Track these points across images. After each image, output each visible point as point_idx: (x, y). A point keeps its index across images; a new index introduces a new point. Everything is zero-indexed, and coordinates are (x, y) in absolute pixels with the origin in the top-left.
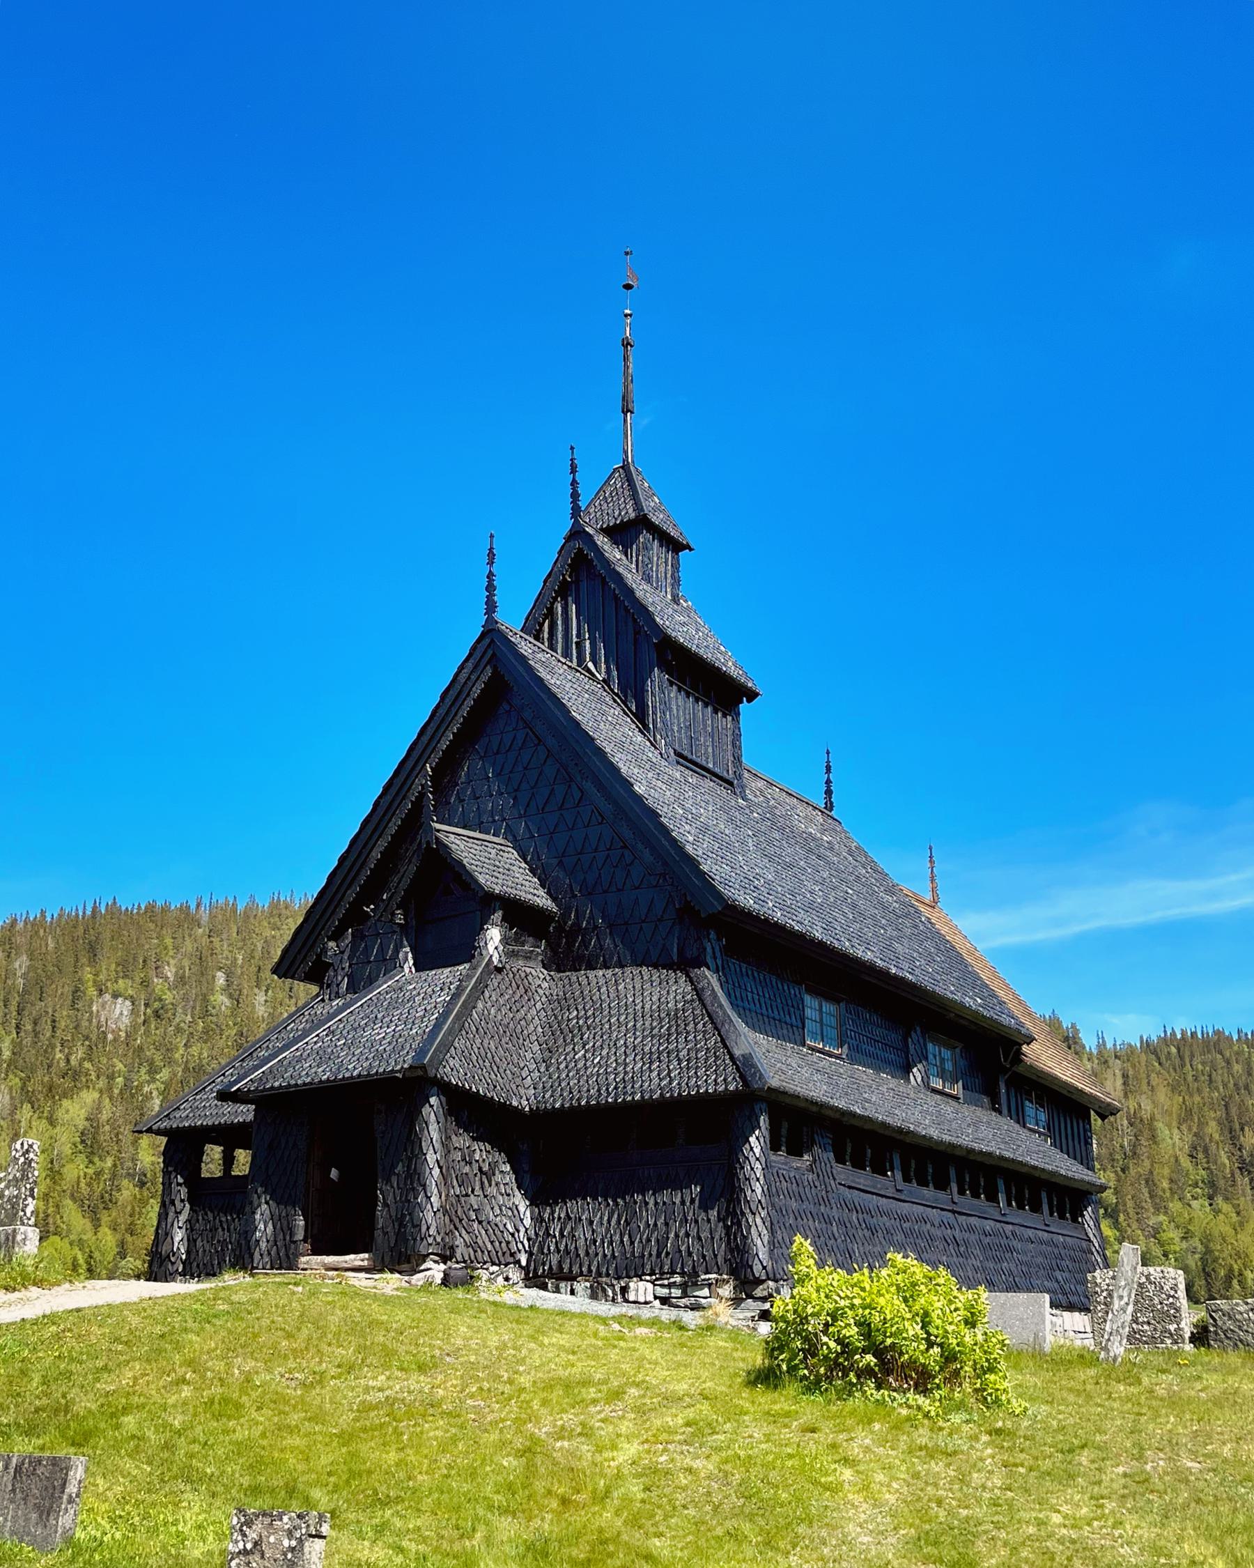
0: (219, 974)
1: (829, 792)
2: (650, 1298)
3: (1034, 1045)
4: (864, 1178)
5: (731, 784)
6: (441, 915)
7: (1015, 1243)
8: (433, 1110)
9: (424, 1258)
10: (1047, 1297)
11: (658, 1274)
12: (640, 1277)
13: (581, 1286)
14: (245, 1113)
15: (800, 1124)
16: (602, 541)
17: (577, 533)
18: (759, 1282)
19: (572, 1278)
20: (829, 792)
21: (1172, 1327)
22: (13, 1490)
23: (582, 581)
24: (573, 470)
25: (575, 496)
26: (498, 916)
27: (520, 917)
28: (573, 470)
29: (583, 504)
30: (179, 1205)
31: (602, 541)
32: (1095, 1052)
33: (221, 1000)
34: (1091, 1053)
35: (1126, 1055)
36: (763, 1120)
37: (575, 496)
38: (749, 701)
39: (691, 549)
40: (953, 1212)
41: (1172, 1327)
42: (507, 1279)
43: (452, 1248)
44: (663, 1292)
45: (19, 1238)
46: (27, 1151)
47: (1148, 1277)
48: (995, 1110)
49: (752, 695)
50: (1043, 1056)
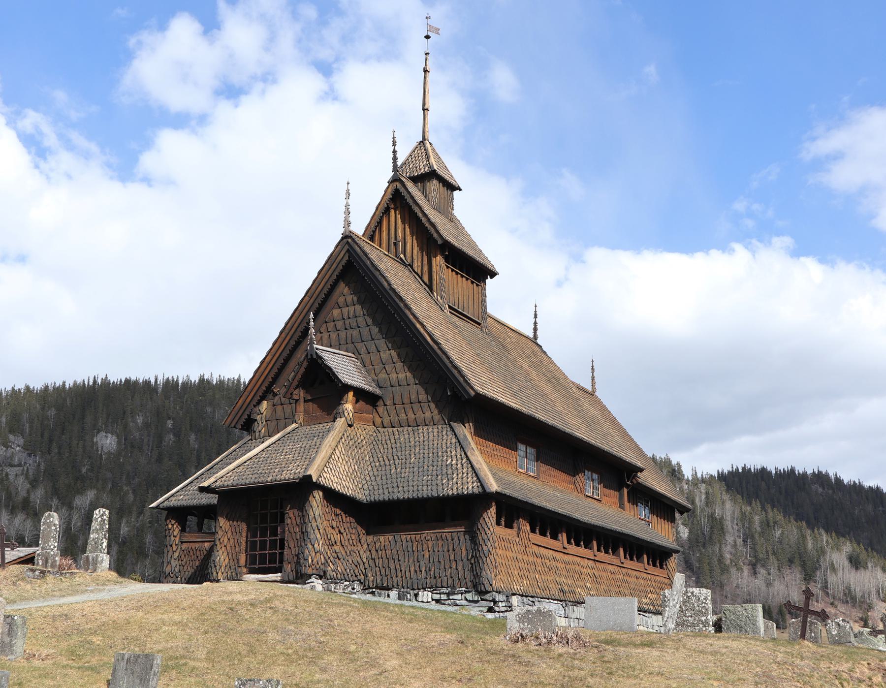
0: (169, 422)
1: (535, 329)
2: (430, 600)
3: (644, 473)
4: (547, 541)
5: (479, 324)
6: (323, 391)
7: (628, 579)
8: (318, 495)
9: (310, 577)
10: (636, 599)
11: (434, 588)
12: (424, 589)
13: (394, 594)
14: (213, 499)
15: (512, 510)
16: (410, 185)
17: (395, 180)
18: (487, 592)
19: (388, 589)
20: (535, 329)
21: (703, 619)
22: (126, 669)
23: (397, 201)
24: (394, 144)
25: (395, 159)
26: (351, 394)
27: (361, 394)
28: (394, 144)
29: (399, 163)
30: (175, 548)
31: (410, 185)
32: (690, 478)
33: (170, 438)
34: (688, 480)
35: (709, 481)
36: (494, 504)
37: (395, 159)
38: (491, 278)
39: (460, 190)
40: (594, 560)
41: (703, 619)
42: (353, 589)
43: (325, 572)
44: (437, 597)
45: (99, 559)
46: (103, 515)
47: (692, 593)
48: (620, 507)
49: (493, 274)
50: (650, 479)
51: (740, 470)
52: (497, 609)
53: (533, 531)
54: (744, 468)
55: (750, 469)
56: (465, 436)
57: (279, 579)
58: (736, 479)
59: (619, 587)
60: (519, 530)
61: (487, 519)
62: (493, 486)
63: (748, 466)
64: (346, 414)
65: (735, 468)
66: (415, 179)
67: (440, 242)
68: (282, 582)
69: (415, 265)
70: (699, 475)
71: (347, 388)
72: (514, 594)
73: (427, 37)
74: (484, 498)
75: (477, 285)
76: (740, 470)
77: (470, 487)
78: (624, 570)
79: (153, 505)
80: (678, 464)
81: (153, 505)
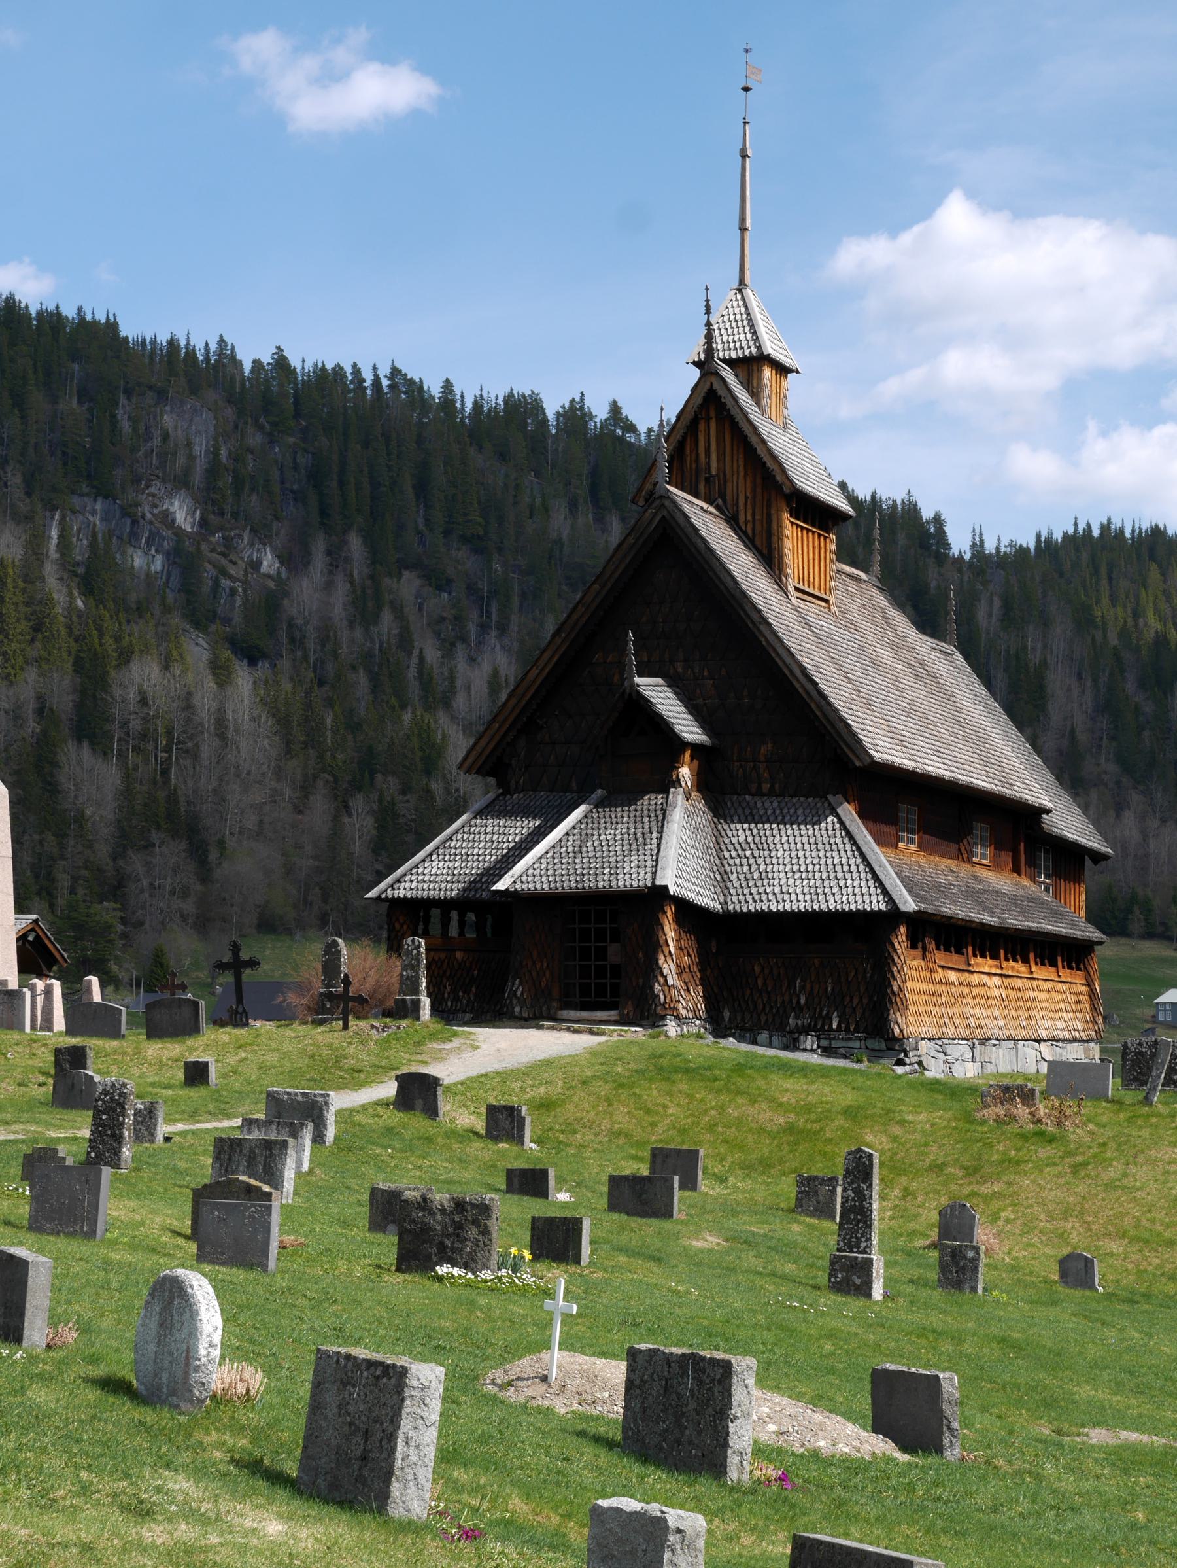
2: (815, 1047)
16: (727, 374)
24: (708, 311)
28: (708, 311)
31: (727, 374)
39: (797, 372)
44: (824, 1043)
51: (1096, 533)
52: (907, 1060)
53: (938, 949)
54: (1105, 528)
55: (1122, 531)
56: (1163, 1063)
57: (613, 1018)
58: (1085, 556)
59: (1028, 1009)
60: (924, 950)
61: (896, 944)
62: (908, 904)
63: (1116, 523)
64: (683, 784)
65: (1082, 526)
66: (730, 362)
67: (786, 490)
68: (617, 1023)
69: (742, 519)
70: (990, 547)
71: (683, 745)
72: (923, 1039)
73: (746, 89)
74: (893, 916)
75: (825, 538)
76: (1096, 533)
77: (876, 903)
78: (1035, 983)
79: (372, 894)
80: (938, 520)
81: (372, 894)
